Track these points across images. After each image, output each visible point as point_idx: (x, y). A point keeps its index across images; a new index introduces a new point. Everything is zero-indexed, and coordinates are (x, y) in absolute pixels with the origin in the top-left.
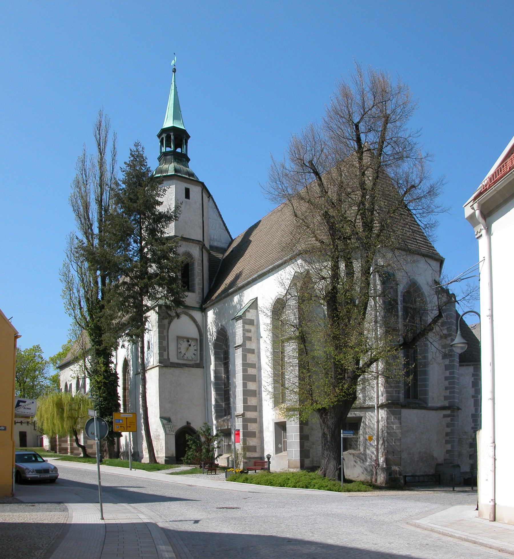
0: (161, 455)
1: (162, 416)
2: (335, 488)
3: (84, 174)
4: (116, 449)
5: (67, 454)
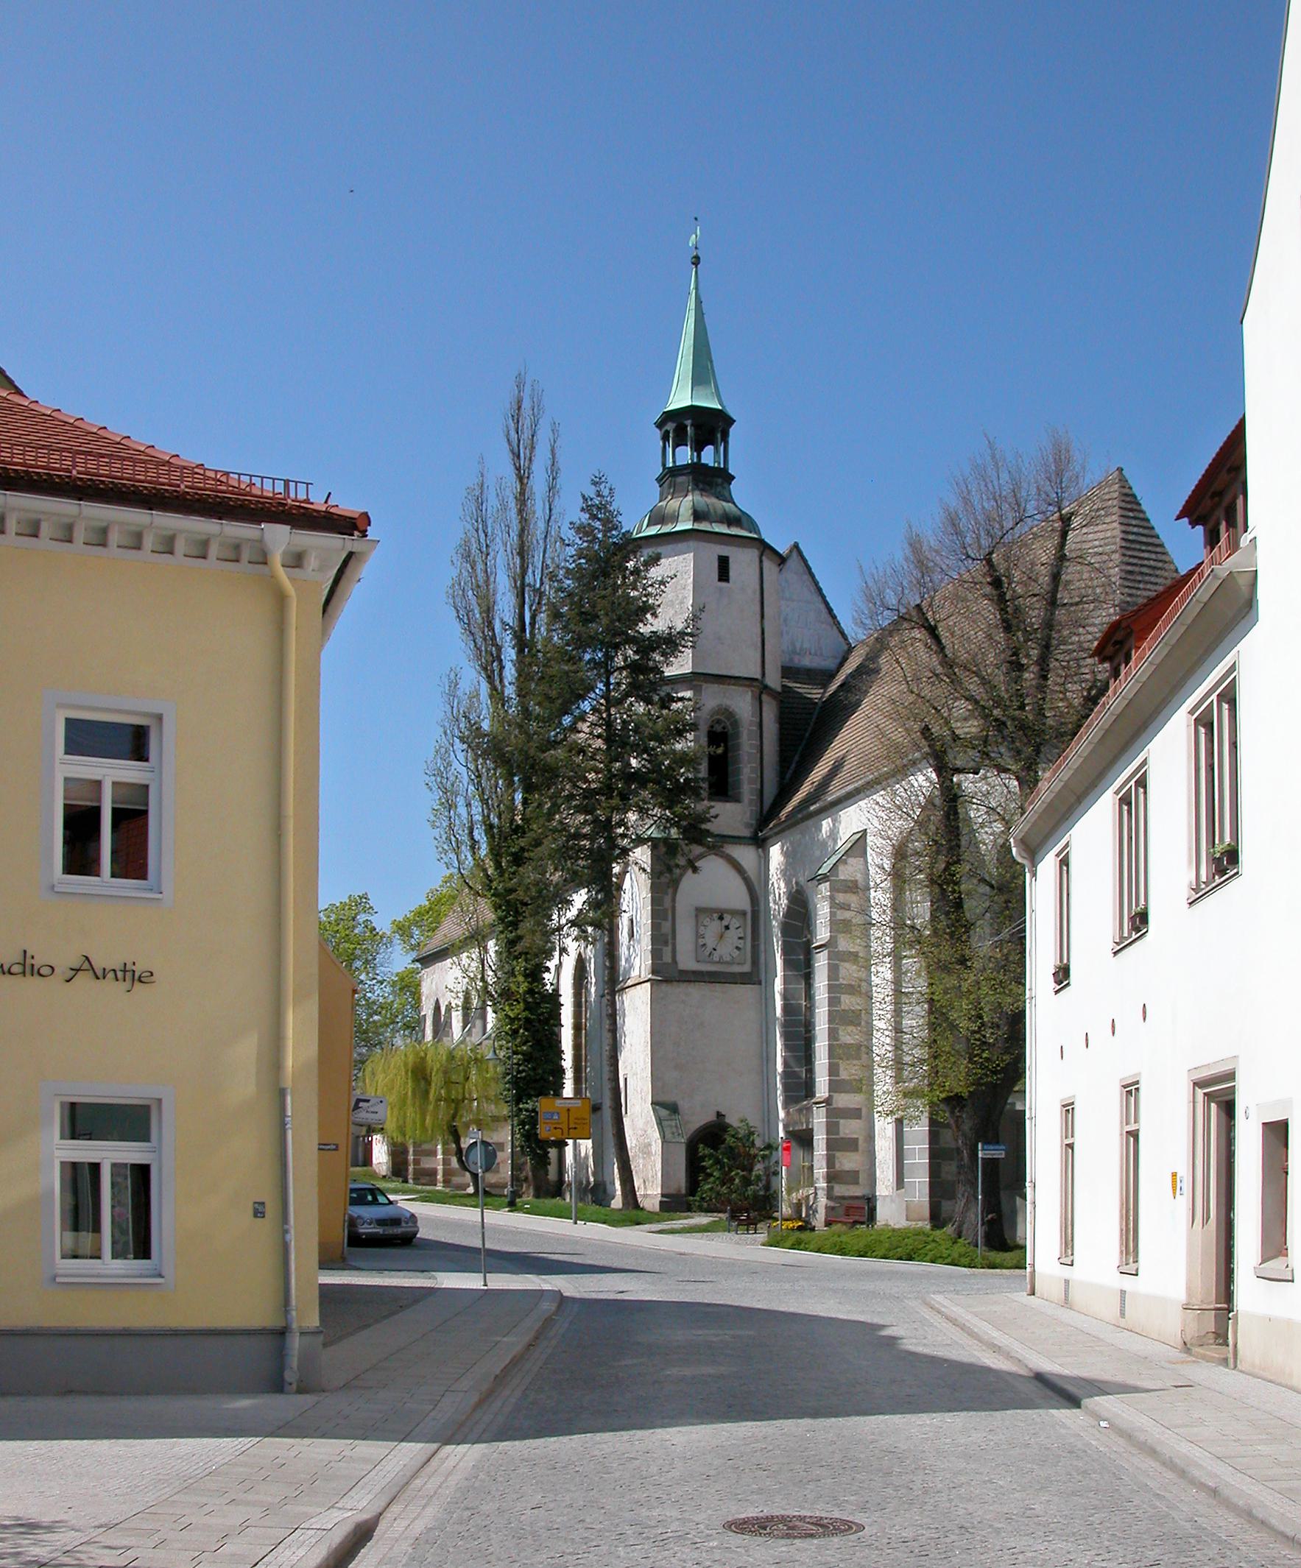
0: (650, 1189)
2: (963, 1260)
3: (481, 532)
5: (436, 1185)
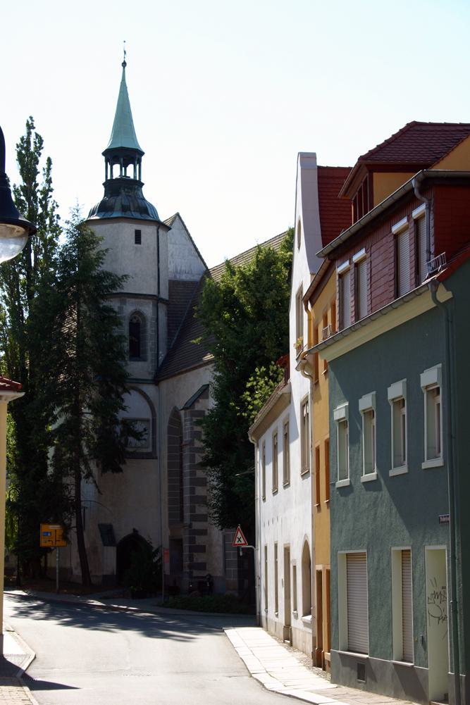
4: (43, 564)
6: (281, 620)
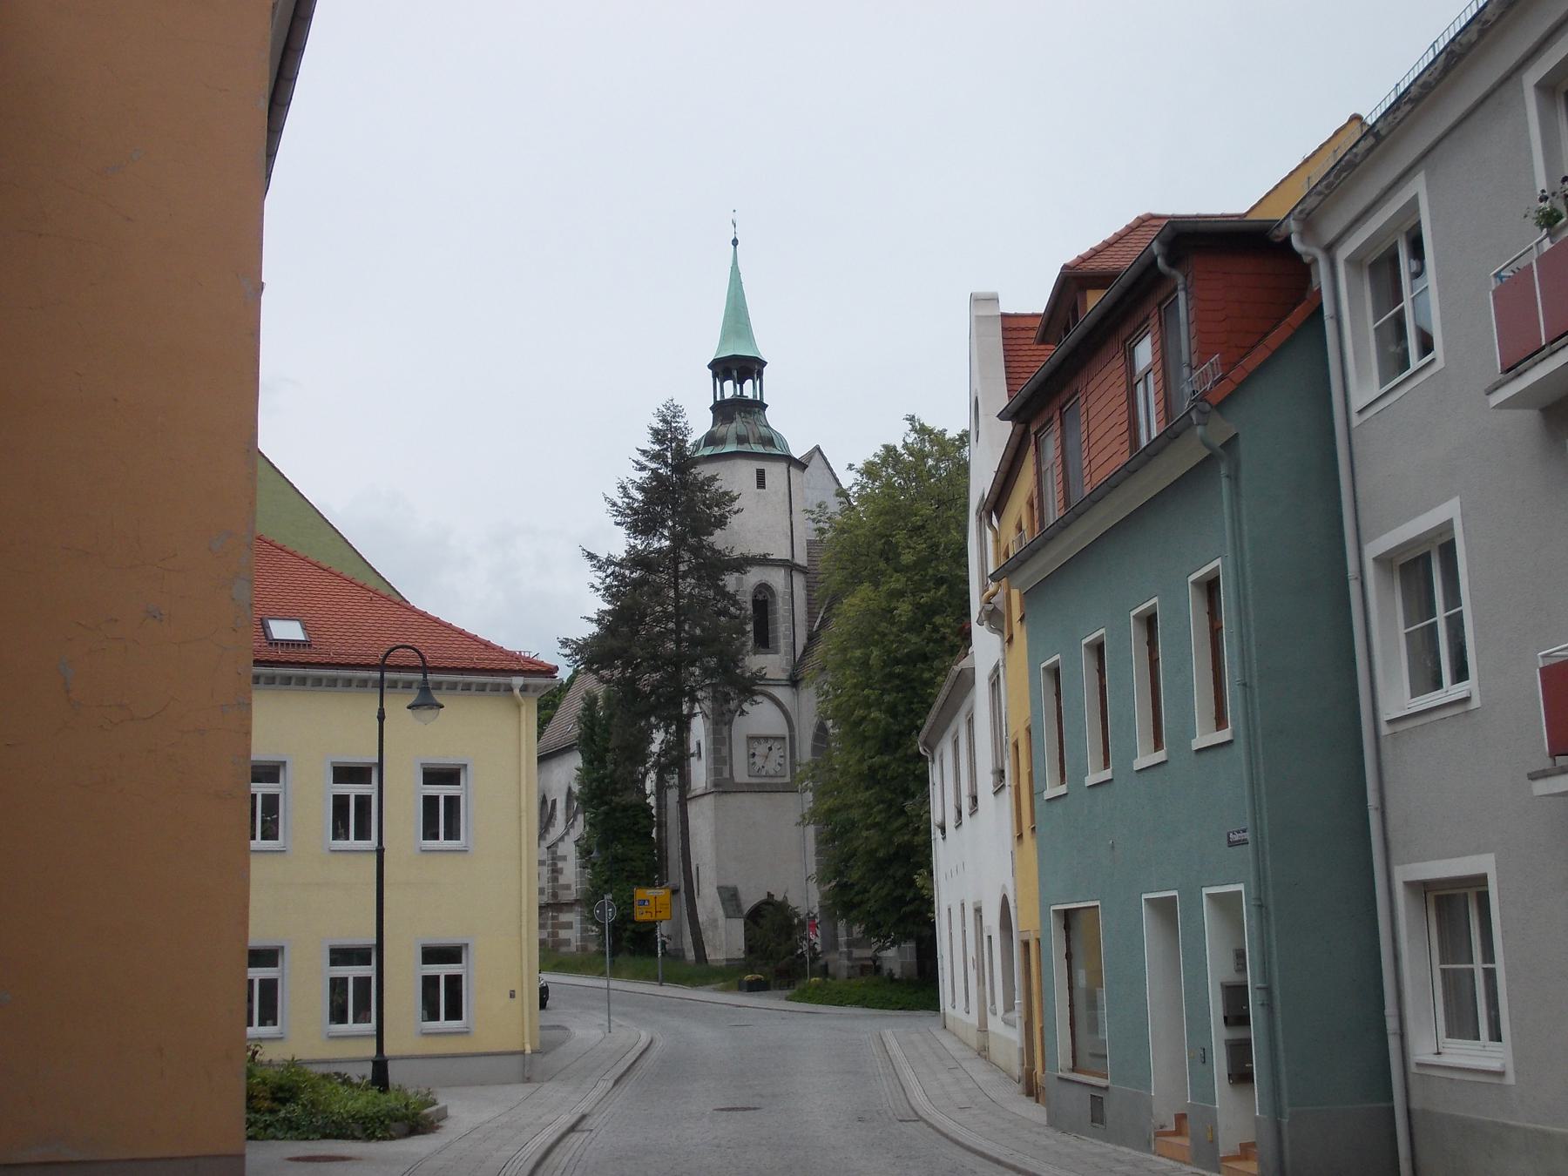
1: (721, 884)
6: (973, 1019)
